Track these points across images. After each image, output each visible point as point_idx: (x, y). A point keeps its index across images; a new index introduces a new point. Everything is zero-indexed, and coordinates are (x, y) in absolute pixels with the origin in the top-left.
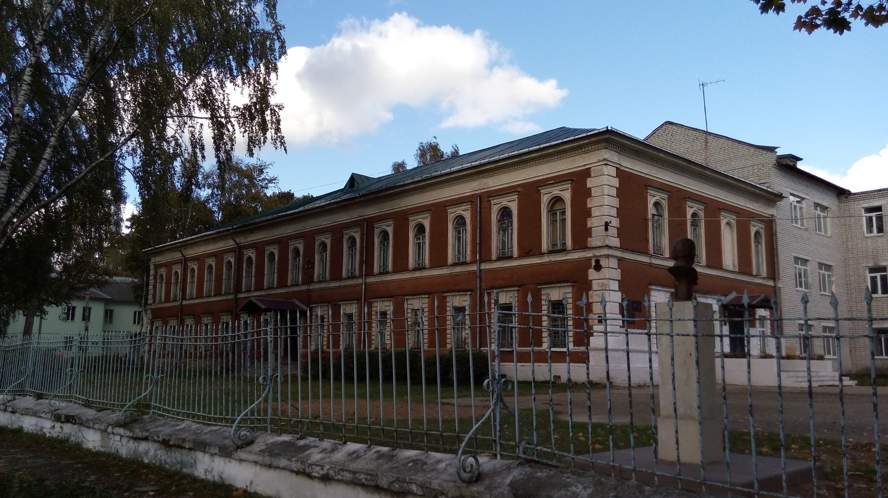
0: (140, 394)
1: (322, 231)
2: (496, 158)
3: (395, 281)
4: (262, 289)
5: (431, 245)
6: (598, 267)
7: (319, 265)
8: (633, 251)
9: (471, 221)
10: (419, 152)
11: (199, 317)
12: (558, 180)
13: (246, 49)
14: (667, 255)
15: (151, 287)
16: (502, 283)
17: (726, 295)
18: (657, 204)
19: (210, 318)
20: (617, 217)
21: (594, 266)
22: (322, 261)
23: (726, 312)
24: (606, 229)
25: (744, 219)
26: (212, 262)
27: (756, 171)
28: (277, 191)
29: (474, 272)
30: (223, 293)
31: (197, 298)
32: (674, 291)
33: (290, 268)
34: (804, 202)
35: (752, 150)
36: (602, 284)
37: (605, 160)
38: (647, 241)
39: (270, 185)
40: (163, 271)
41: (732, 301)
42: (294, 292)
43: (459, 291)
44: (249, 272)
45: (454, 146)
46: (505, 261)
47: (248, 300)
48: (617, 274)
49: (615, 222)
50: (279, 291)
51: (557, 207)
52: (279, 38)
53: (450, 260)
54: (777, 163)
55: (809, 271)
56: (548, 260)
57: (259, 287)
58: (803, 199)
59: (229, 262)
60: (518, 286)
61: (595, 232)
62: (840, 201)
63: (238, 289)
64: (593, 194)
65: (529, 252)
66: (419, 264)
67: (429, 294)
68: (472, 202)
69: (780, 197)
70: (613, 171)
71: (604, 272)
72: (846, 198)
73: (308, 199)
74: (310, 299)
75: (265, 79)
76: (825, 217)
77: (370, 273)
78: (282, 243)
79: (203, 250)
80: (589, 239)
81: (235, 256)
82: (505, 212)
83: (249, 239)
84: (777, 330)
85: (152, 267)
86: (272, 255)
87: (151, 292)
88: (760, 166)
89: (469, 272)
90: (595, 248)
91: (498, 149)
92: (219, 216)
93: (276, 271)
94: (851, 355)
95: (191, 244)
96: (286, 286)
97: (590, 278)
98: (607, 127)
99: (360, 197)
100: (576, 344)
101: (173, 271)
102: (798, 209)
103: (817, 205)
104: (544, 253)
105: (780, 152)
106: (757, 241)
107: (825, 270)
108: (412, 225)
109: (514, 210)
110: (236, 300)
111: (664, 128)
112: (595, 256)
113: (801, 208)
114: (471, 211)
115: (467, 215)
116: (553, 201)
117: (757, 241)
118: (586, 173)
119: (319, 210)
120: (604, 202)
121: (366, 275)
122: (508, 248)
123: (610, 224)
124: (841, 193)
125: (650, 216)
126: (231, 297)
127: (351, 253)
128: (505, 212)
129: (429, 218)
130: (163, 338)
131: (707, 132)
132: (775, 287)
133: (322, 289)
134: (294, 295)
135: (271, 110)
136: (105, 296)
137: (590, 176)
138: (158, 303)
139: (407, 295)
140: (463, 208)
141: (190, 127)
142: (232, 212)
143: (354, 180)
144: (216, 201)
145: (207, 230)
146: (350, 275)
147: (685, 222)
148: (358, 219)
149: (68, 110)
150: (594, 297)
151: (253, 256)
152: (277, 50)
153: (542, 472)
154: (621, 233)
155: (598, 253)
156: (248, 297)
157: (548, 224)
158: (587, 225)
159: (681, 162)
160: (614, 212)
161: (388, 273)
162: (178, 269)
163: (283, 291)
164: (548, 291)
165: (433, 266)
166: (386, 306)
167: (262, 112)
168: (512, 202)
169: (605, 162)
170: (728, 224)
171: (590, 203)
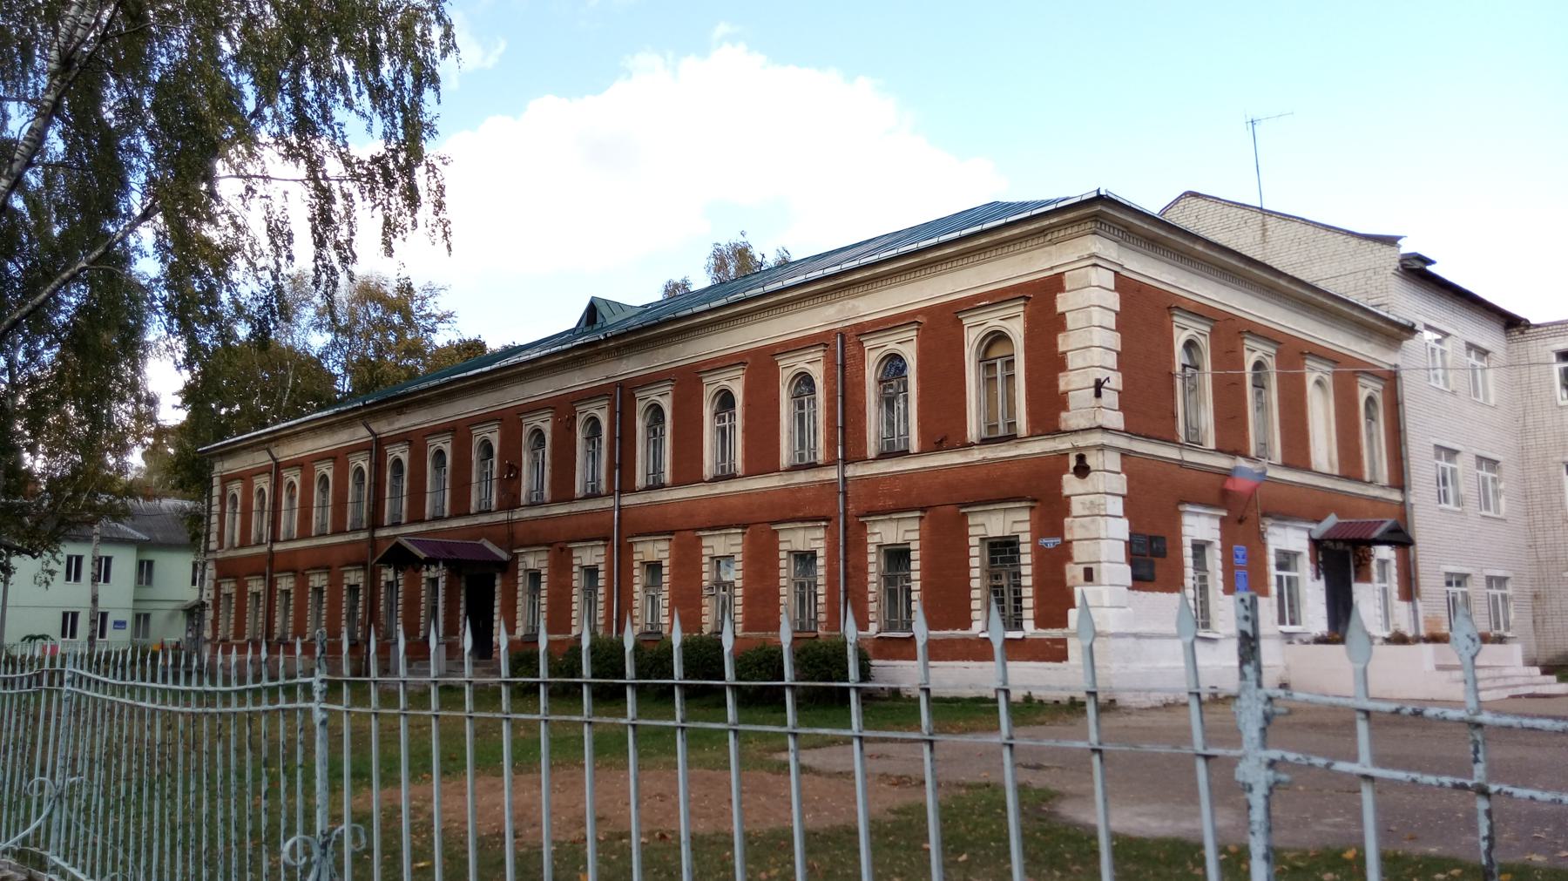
0: (27, 824)
1: (534, 408)
2: (875, 258)
4: (422, 521)
5: (746, 430)
6: (1082, 470)
7: (530, 472)
8: (1148, 437)
9: (826, 382)
10: (712, 260)
11: (303, 574)
12: (999, 298)
13: (375, 40)
14: (1211, 444)
15: (214, 519)
16: (890, 503)
17: (1318, 521)
18: (1190, 345)
19: (325, 577)
20: (1118, 370)
21: (1075, 468)
22: (537, 465)
23: (1320, 553)
24: (1098, 394)
25: (1347, 373)
26: (327, 469)
27: (1362, 282)
28: (455, 339)
29: (832, 483)
30: (348, 529)
31: (299, 539)
32: (1224, 513)
33: (474, 479)
34: (1448, 341)
35: (1354, 242)
36: (1092, 503)
37: (1091, 256)
38: (1174, 417)
39: (439, 326)
40: (236, 488)
41: (1329, 532)
42: (480, 526)
43: (803, 520)
44: (396, 489)
45: (781, 250)
46: (894, 461)
47: (393, 543)
48: (1120, 483)
49: (1116, 381)
50: (455, 524)
51: (997, 351)
52: (440, 18)
53: (784, 461)
54: (1403, 266)
55: (1460, 474)
56: (980, 457)
57: (416, 517)
58: (1446, 335)
59: (359, 470)
60: (922, 509)
61: (1074, 400)
62: (1510, 339)
63: (375, 522)
64: (1070, 324)
65: (941, 441)
66: (723, 468)
67: (745, 526)
68: (827, 345)
69: (1410, 330)
70: (1108, 279)
71: (1096, 481)
72: (1522, 333)
73: (509, 351)
74: (512, 538)
75: (412, 100)
76: (1483, 369)
77: (628, 487)
78: (459, 431)
79: (311, 448)
80: (1063, 415)
81: (371, 458)
82: (804, 380)
83: (397, 425)
84: (1409, 589)
85: (216, 481)
86: (440, 454)
87: (215, 527)
88: (1370, 273)
89: (823, 484)
90: (1075, 432)
91: (872, 246)
92: (344, 385)
93: (447, 486)
94: (1535, 630)
95: (287, 436)
96: (468, 514)
97: (1067, 491)
98: (1098, 191)
99: (607, 339)
100: (1040, 622)
101: (256, 488)
102: (1438, 353)
103: (1471, 347)
104: (973, 444)
105: (1406, 247)
106: (1370, 417)
107: (1487, 471)
108: (708, 393)
109: (910, 358)
110: (373, 541)
111: (1182, 203)
112: (1075, 448)
113: (1443, 353)
114: (826, 363)
115: (818, 372)
116: (990, 338)
117: (1370, 417)
118: (1055, 284)
119: (529, 366)
120: (1091, 340)
121: (621, 492)
122: (899, 435)
123: (1106, 384)
124: (1511, 323)
125: (1178, 368)
126: (363, 536)
127: (591, 449)
128: (894, 364)
129: (742, 379)
130: (77, 680)
131: (1261, 209)
132: (1403, 504)
133: (536, 519)
134: (481, 530)
135: (427, 164)
136: (139, 535)
137: (1062, 290)
138: (228, 549)
139: (701, 530)
140: (810, 357)
141: (261, 197)
142: (368, 374)
143: (593, 312)
144: (339, 356)
145: (321, 408)
146: (589, 491)
147: (1242, 377)
148: (604, 382)
149: (15, 166)
150: (1074, 528)
151: (405, 458)
152: (437, 44)
153: (240, 86)
154: (1126, 403)
155: (1081, 441)
156: (395, 536)
157: (978, 387)
158: (1057, 386)
159: (1234, 262)
160: (1112, 360)
161: (662, 486)
162: (264, 483)
163: (462, 522)
164: (979, 519)
165: (750, 473)
166: (661, 551)
167: (408, 170)
168: (905, 344)
169: (1094, 261)
170: (1319, 383)
171: (1064, 343)
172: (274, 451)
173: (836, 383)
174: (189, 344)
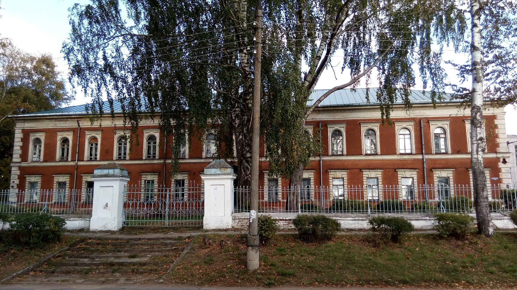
3: (350, 160)
16: (441, 166)
32: (129, 180)
60: (42, 175)
82: (65, 141)
155: (505, 155)
172: (80, 123)
173: (424, 133)
174: (429, 36)
